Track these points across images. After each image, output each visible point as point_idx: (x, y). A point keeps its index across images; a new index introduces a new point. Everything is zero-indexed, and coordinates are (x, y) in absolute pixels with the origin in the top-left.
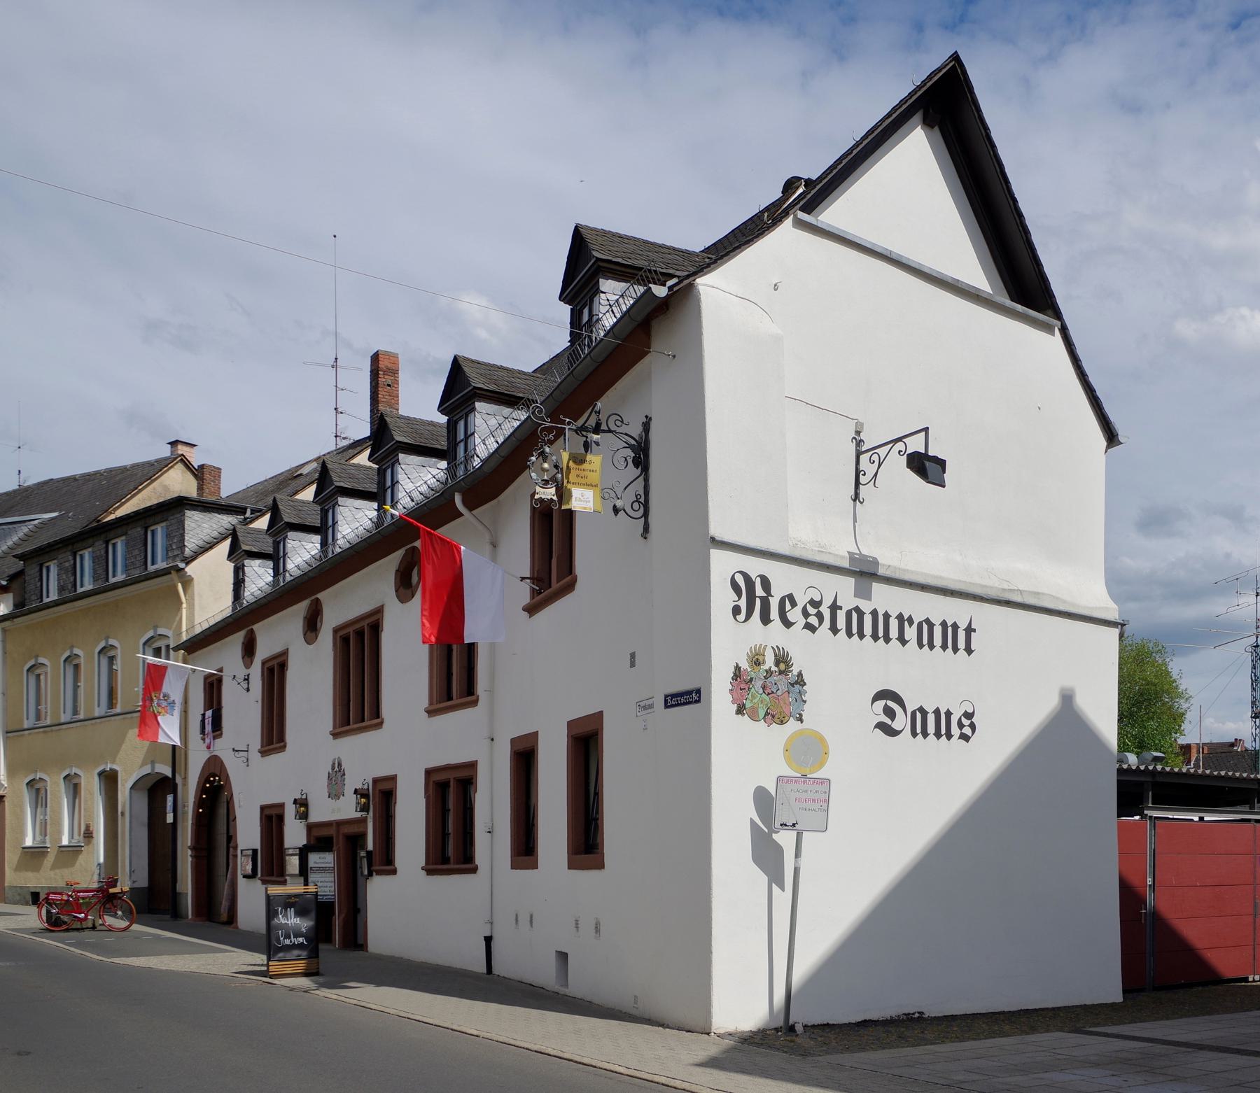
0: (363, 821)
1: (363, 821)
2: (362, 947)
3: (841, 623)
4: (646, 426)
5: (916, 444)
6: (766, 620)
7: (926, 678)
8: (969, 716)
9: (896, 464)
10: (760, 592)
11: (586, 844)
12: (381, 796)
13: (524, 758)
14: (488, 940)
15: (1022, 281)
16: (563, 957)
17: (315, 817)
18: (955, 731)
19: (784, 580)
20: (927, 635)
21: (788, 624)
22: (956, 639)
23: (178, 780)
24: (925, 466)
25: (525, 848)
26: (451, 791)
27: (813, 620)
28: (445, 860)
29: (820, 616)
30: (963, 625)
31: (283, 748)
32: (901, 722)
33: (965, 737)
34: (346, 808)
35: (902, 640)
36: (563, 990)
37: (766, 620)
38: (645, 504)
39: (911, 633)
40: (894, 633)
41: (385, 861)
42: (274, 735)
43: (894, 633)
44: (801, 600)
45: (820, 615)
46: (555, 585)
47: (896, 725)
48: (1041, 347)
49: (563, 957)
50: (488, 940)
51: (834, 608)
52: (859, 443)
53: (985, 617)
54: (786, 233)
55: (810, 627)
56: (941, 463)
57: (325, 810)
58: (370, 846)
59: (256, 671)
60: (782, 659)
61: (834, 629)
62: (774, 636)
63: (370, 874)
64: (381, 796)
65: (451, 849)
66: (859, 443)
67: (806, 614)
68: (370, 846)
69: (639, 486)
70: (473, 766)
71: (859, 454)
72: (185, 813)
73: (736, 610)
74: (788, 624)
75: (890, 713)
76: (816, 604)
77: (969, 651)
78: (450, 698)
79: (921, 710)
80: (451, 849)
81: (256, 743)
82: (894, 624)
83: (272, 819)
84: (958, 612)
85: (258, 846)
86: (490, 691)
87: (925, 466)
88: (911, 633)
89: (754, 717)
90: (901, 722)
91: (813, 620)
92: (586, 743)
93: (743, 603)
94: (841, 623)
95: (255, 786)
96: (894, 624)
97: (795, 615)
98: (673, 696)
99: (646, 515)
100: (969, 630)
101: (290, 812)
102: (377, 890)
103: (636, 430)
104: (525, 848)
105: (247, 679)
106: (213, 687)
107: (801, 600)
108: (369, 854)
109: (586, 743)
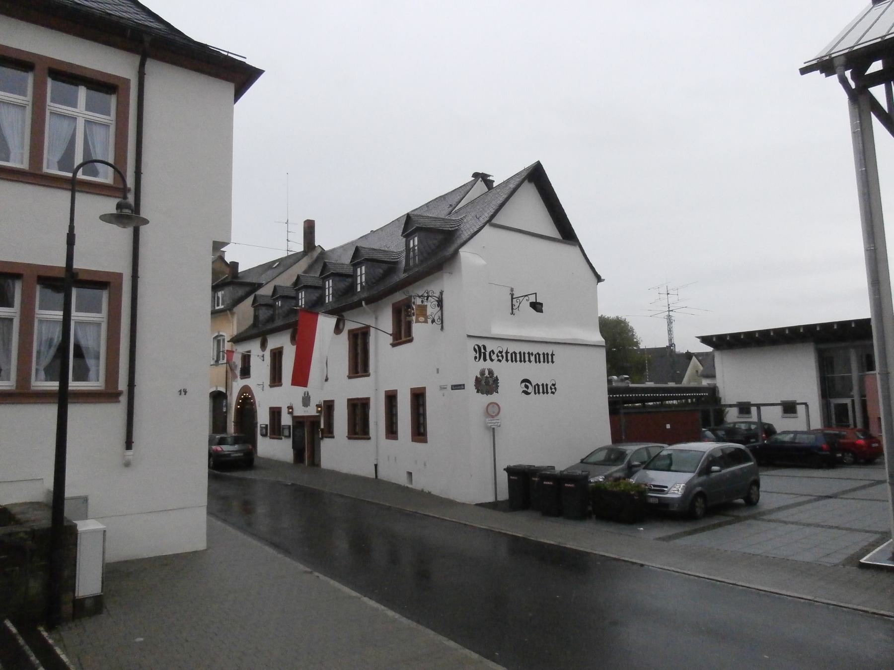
0: (319, 417)
1: (319, 417)
2: (319, 465)
3: (509, 358)
4: (441, 293)
5: (532, 299)
6: (485, 360)
7: (538, 373)
8: (554, 385)
9: (525, 305)
10: (483, 351)
11: (419, 432)
12: (328, 407)
13: (391, 398)
14: (376, 466)
15: (567, 234)
16: (410, 474)
17: (296, 414)
18: (549, 391)
19: (490, 346)
20: (538, 358)
21: (492, 360)
22: (548, 358)
23: (228, 394)
24: (537, 306)
25: (392, 431)
26: (359, 410)
27: (500, 358)
28: (356, 433)
29: (502, 356)
30: (550, 353)
31: (281, 385)
32: (531, 389)
33: (553, 393)
34: (312, 411)
35: (530, 361)
36: (410, 486)
37: (485, 360)
38: (442, 319)
39: (532, 358)
40: (527, 359)
41: (329, 432)
42: (276, 379)
43: (527, 359)
44: (496, 352)
45: (504, 356)
46: (403, 339)
47: (529, 391)
48: (573, 251)
49: (410, 474)
50: (376, 466)
51: (507, 353)
52: (512, 295)
53: (557, 350)
54: (487, 227)
55: (499, 361)
56: (541, 304)
57: (300, 411)
58: (322, 426)
59: (267, 354)
60: (491, 372)
61: (507, 360)
62: (488, 365)
63: (322, 438)
64: (328, 407)
65: (359, 427)
66: (512, 295)
67: (498, 356)
68: (322, 426)
69: (440, 313)
70: (368, 399)
71: (512, 299)
72: (231, 407)
73: (476, 358)
74: (492, 360)
75: (527, 387)
76: (501, 352)
77: (553, 362)
78: (357, 372)
79: (538, 385)
80: (359, 427)
81: (267, 381)
82: (527, 356)
83: (275, 413)
84: (548, 349)
85: (268, 423)
86: (376, 372)
87: (537, 306)
88: (532, 358)
89: (482, 393)
90: (531, 389)
91: (500, 358)
92: (418, 397)
93: (478, 355)
94: (509, 358)
95: (266, 399)
96: (527, 356)
97: (494, 357)
98: (455, 386)
99: (442, 323)
100: (552, 355)
101: (284, 412)
102: (326, 445)
103: (437, 294)
104: (392, 431)
105: (263, 356)
106: (246, 358)
107: (496, 352)
108: (322, 430)
109: (418, 397)
